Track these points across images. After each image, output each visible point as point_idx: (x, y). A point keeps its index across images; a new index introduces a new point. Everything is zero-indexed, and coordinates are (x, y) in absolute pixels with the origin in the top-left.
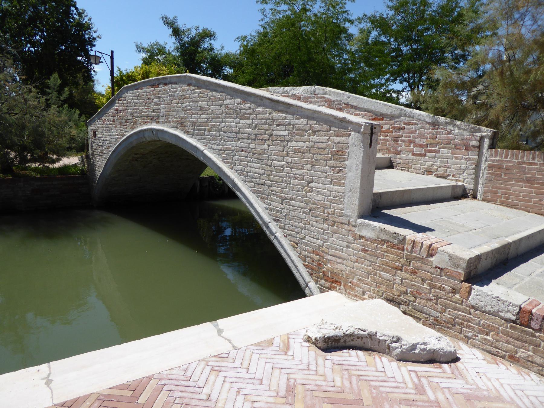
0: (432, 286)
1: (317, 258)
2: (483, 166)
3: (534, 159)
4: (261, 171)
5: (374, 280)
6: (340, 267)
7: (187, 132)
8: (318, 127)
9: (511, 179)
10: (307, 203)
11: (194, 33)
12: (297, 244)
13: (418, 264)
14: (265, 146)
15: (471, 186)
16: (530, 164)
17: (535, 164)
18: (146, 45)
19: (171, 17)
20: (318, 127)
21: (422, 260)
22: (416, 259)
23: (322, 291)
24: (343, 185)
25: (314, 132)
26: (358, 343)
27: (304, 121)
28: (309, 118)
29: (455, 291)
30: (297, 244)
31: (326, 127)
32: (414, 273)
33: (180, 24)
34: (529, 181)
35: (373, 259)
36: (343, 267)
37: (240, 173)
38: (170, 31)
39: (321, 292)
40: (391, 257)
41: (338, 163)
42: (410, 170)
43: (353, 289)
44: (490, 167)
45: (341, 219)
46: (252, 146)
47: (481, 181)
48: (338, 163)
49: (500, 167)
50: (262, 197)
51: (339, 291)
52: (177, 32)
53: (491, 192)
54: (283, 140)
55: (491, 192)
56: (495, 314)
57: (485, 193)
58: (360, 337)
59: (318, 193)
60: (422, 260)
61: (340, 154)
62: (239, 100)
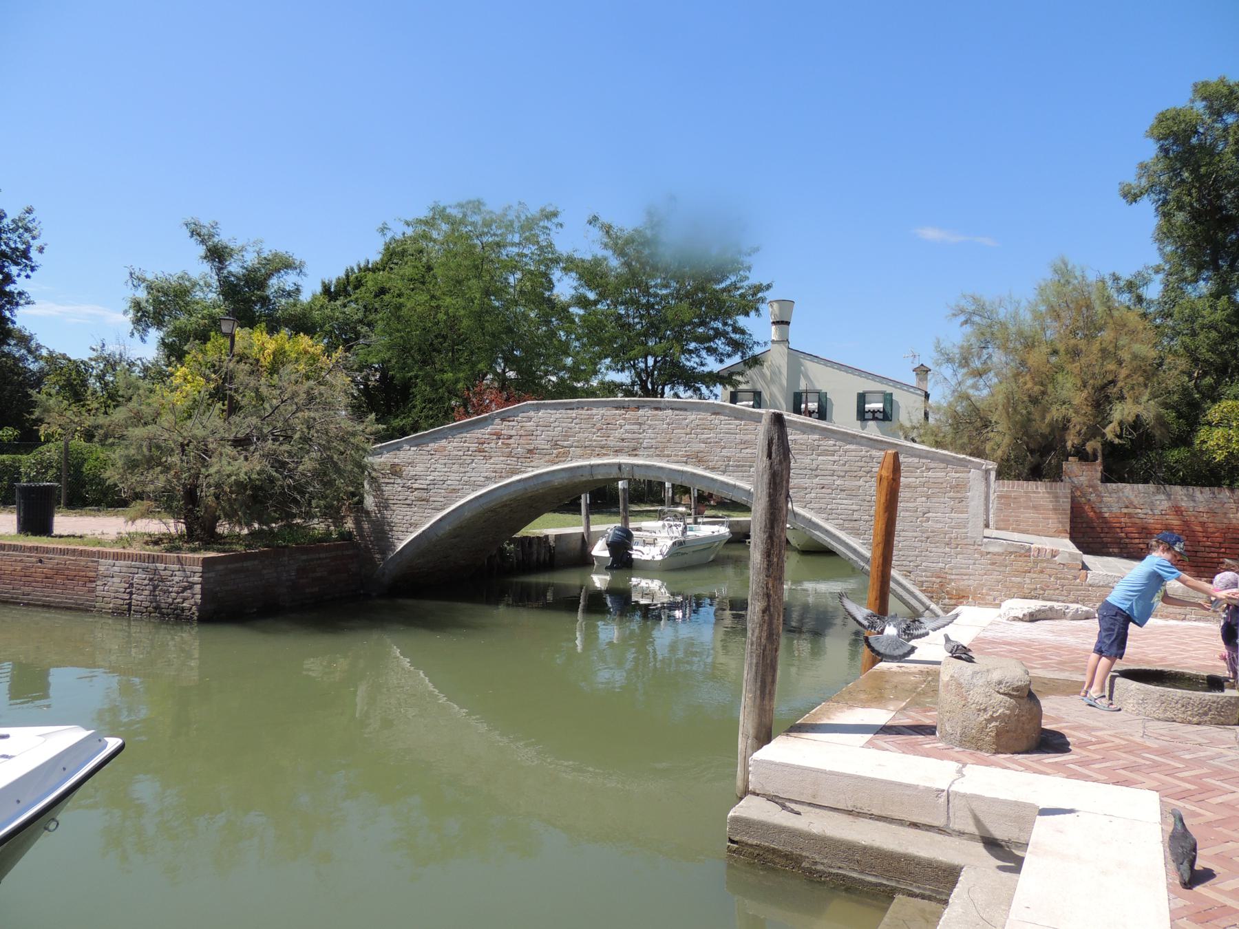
0: (1057, 578)
1: (938, 580)
2: (992, 497)
4: (854, 507)
5: (1006, 587)
6: (966, 583)
7: (713, 469)
8: (932, 465)
11: (251, 259)
14: (861, 482)
18: (150, 277)
19: (206, 221)
20: (932, 465)
21: (1048, 561)
22: (1042, 561)
25: (929, 469)
26: (1043, 615)
27: (916, 460)
28: (920, 457)
29: (1075, 578)
31: (943, 465)
32: (1042, 572)
33: (224, 237)
34: (1035, 508)
35: (1002, 569)
36: (971, 582)
37: (819, 511)
38: (202, 250)
40: (1020, 564)
41: (959, 495)
42: (146, 538)
43: (983, 599)
44: (1000, 497)
45: (965, 542)
47: (992, 511)
48: (959, 495)
51: (968, 604)
52: (217, 255)
57: (996, 522)
58: (1044, 611)
59: (938, 522)
60: (1048, 561)
61: (960, 487)
62: (817, 437)
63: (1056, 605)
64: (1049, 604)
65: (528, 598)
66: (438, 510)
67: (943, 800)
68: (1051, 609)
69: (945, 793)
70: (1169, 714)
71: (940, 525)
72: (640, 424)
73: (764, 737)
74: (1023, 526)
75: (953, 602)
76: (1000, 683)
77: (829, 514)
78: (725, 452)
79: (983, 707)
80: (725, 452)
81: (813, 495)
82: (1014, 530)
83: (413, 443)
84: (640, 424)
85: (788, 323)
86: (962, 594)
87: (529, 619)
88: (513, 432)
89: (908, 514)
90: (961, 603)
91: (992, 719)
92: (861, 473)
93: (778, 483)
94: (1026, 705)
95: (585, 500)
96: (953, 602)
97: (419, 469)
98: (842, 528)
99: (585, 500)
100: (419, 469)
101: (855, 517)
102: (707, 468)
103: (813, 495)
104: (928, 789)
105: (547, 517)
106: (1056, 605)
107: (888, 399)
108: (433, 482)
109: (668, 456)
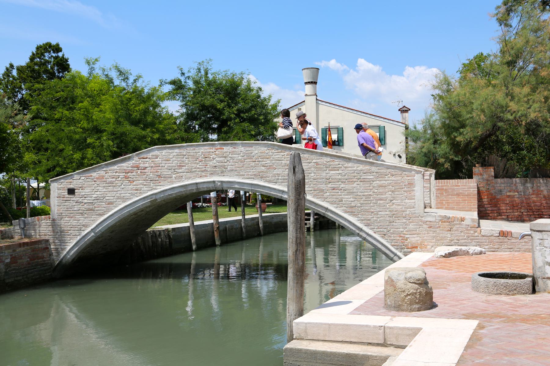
3: (458, 183)
4: (352, 199)
7: (269, 182)
9: (448, 195)
10: (390, 211)
12: (385, 235)
13: (458, 226)
14: (355, 185)
15: (429, 201)
16: (456, 186)
17: (459, 186)
23: (405, 255)
24: (414, 199)
29: (475, 232)
30: (385, 235)
39: (406, 256)
43: (426, 248)
45: (414, 215)
46: (342, 186)
49: (443, 189)
50: (352, 213)
53: (439, 203)
54: (371, 181)
55: (439, 203)
56: (492, 236)
61: (411, 184)
63: (464, 248)
64: (459, 248)
65: (155, 273)
66: (101, 215)
67: (382, 331)
68: (461, 250)
69: (382, 328)
70: (499, 292)
71: (399, 207)
72: (225, 157)
73: (301, 313)
74: (451, 206)
75: (409, 250)
76: (411, 278)
77: (339, 202)
78: (276, 172)
79: (403, 290)
80: (276, 172)
81: (328, 194)
82: (447, 209)
83: (78, 174)
84: (225, 157)
85: (315, 83)
86: (414, 246)
87: (153, 286)
88: (147, 165)
89: (382, 202)
90: (414, 251)
91: (408, 295)
92: (355, 180)
93: (300, 188)
94: (422, 290)
95: (189, 205)
96: (409, 250)
97: (87, 191)
98: (346, 212)
99: (189, 205)
100: (87, 191)
101: (353, 204)
102: (266, 181)
103: (328, 194)
104: (375, 327)
105: (171, 216)
106: (464, 248)
107: (382, 130)
108: (97, 199)
109: (243, 175)
